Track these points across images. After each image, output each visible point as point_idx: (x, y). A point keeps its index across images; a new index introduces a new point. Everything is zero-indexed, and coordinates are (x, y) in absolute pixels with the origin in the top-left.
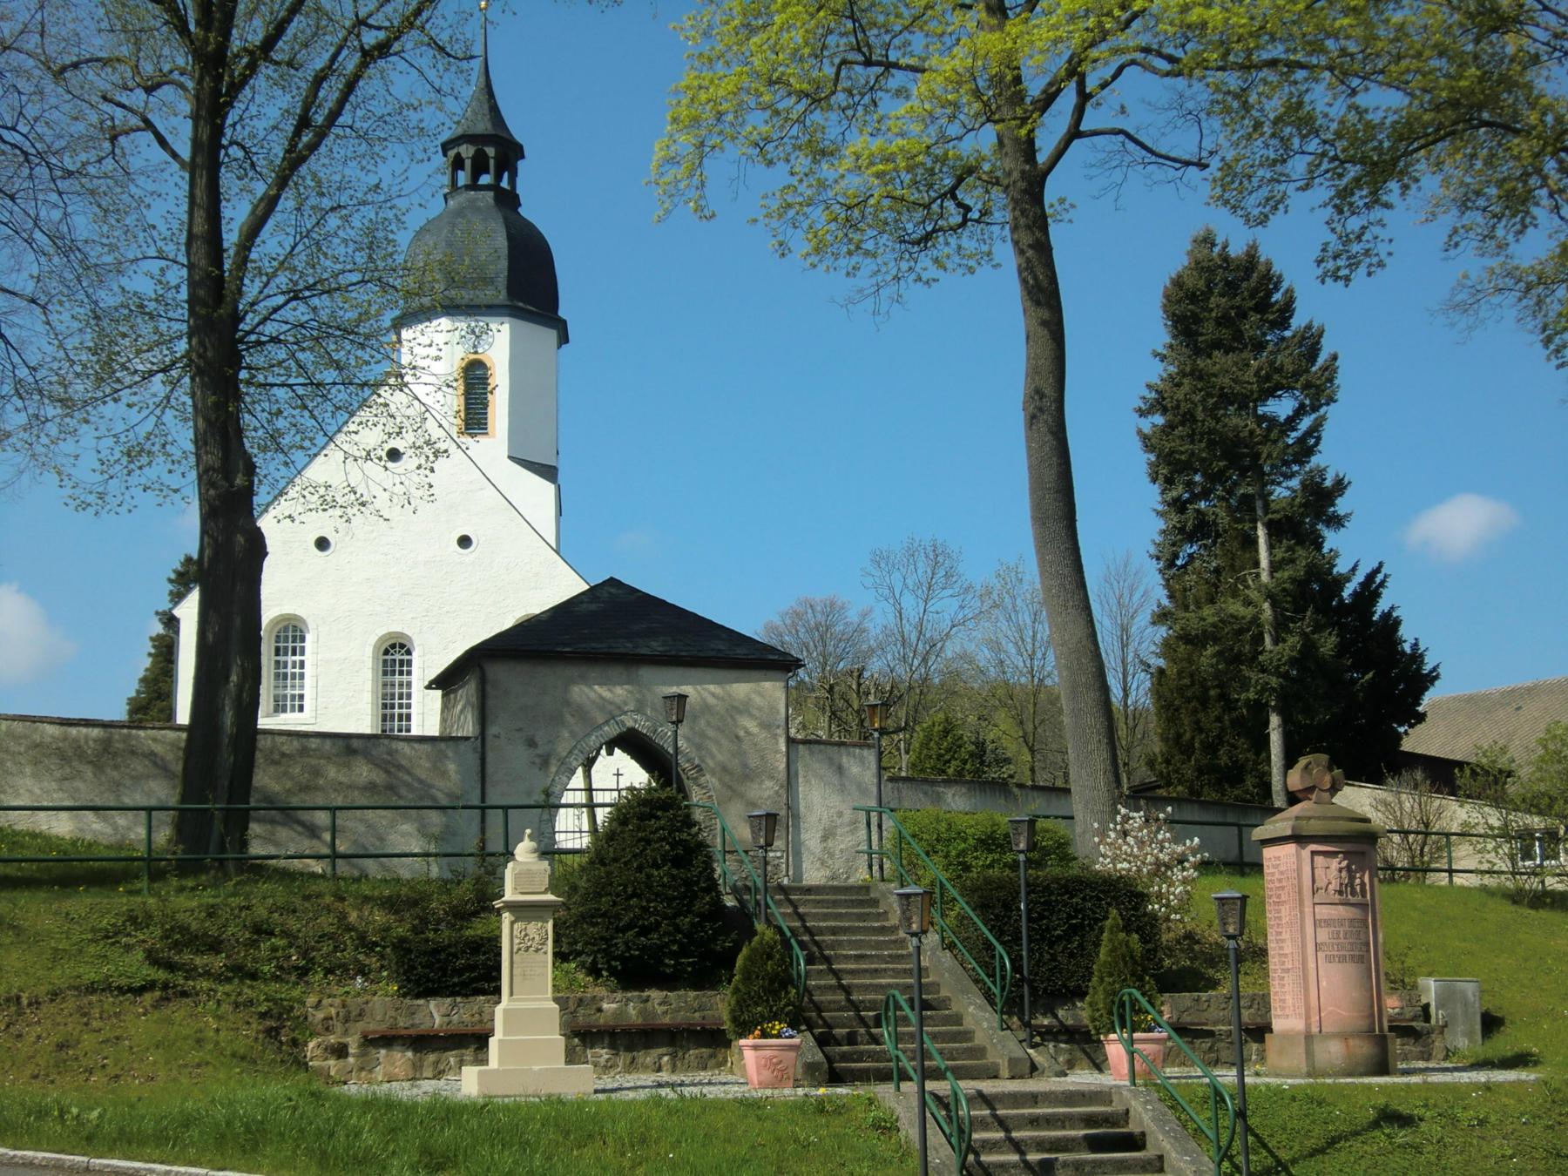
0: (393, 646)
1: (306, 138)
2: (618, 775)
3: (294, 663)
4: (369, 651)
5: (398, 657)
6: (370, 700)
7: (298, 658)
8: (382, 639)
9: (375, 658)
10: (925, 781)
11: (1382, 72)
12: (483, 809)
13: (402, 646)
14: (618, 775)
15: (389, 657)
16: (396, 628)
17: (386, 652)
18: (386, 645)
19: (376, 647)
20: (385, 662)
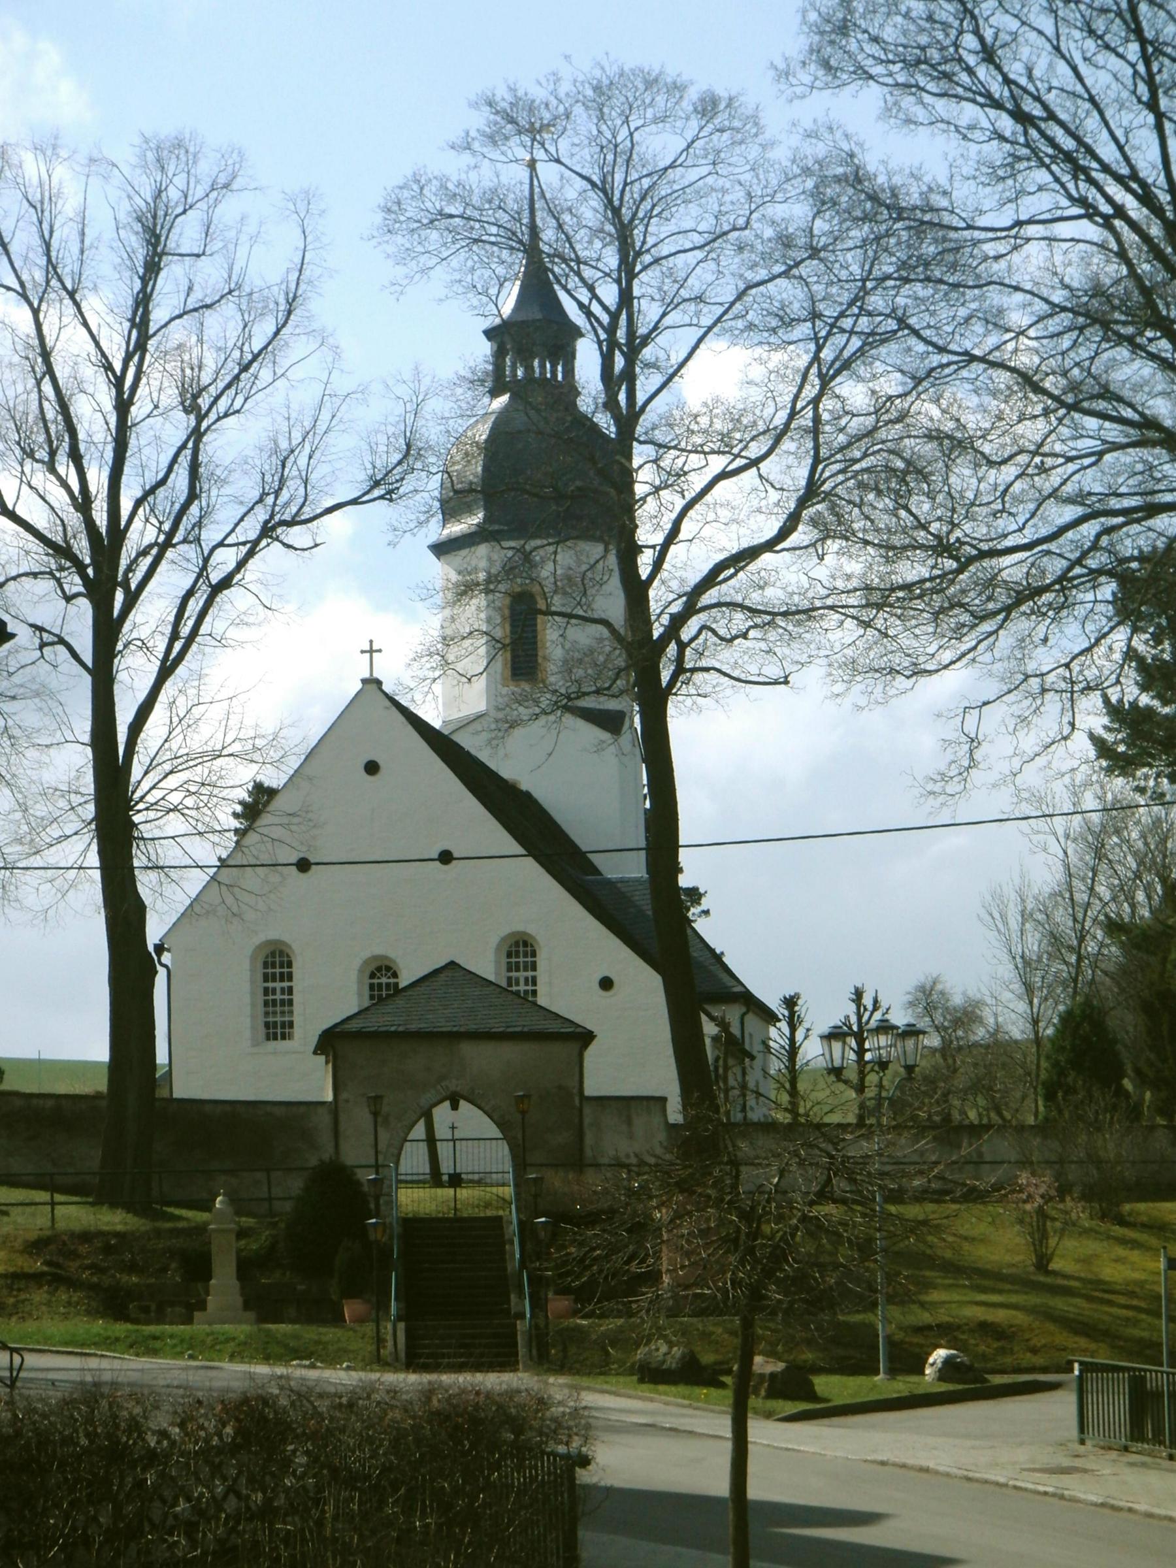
0: (379, 969)
1: (178, 646)
2: (371, 651)
3: (283, 989)
4: (353, 976)
5: (384, 980)
6: (422, 1210)
7: (286, 984)
8: (366, 962)
9: (360, 982)
10: (956, 96)
11: (1118, 682)
12: (454, 1140)
13: (388, 968)
14: (371, 651)
15: (376, 981)
16: (379, 951)
17: (372, 976)
18: (372, 967)
19: (361, 971)
20: (372, 987)
